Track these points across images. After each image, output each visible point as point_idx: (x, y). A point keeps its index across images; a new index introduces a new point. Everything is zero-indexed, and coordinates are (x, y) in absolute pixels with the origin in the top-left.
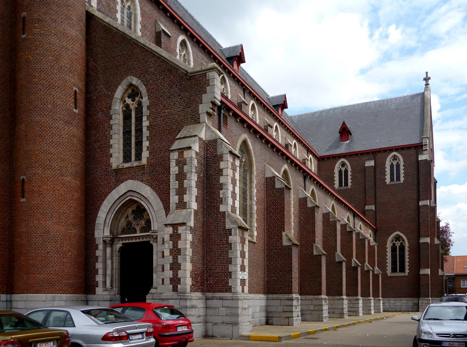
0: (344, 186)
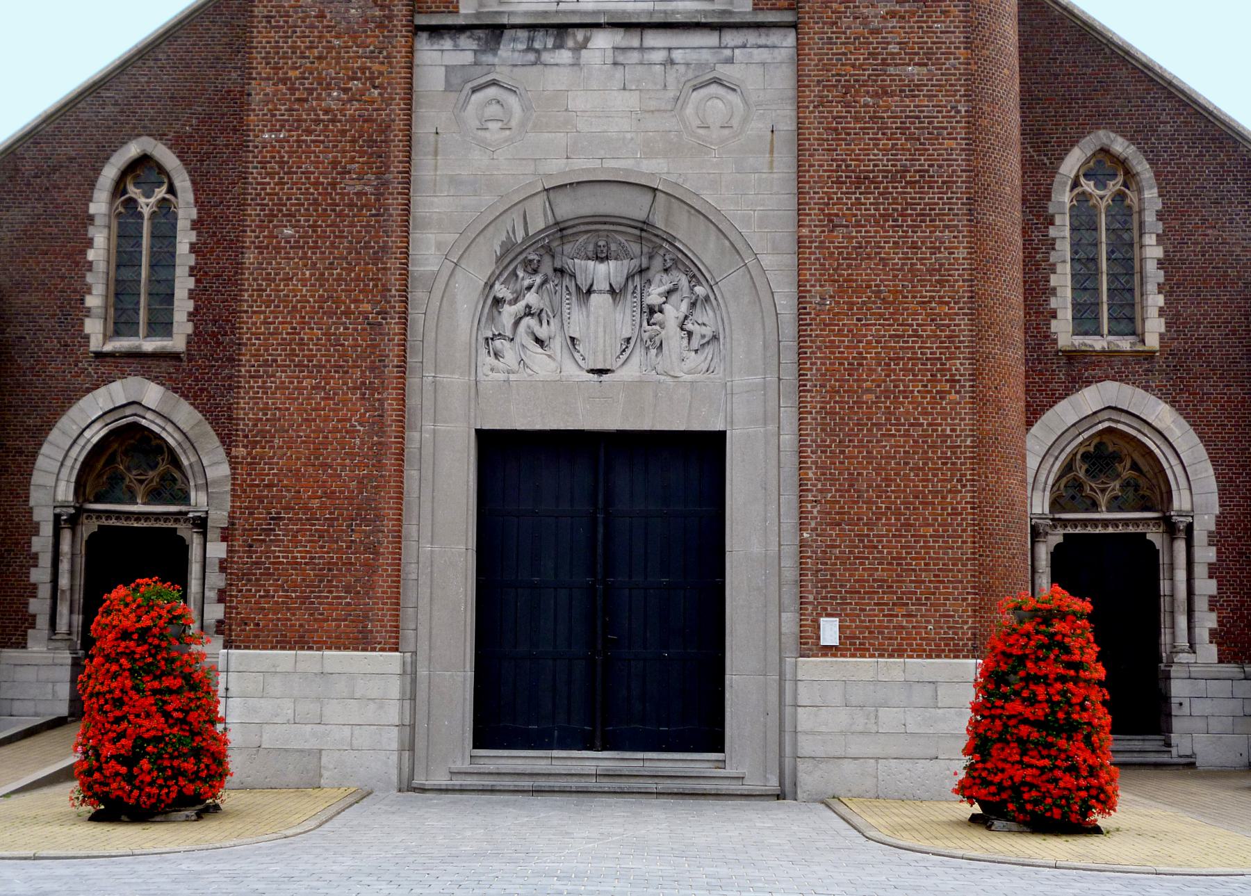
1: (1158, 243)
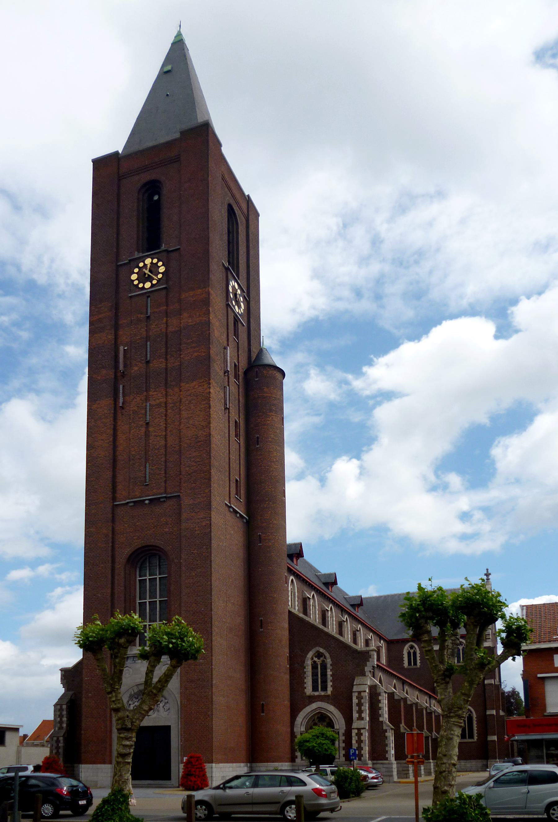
0: (413, 665)
1: (331, 671)
